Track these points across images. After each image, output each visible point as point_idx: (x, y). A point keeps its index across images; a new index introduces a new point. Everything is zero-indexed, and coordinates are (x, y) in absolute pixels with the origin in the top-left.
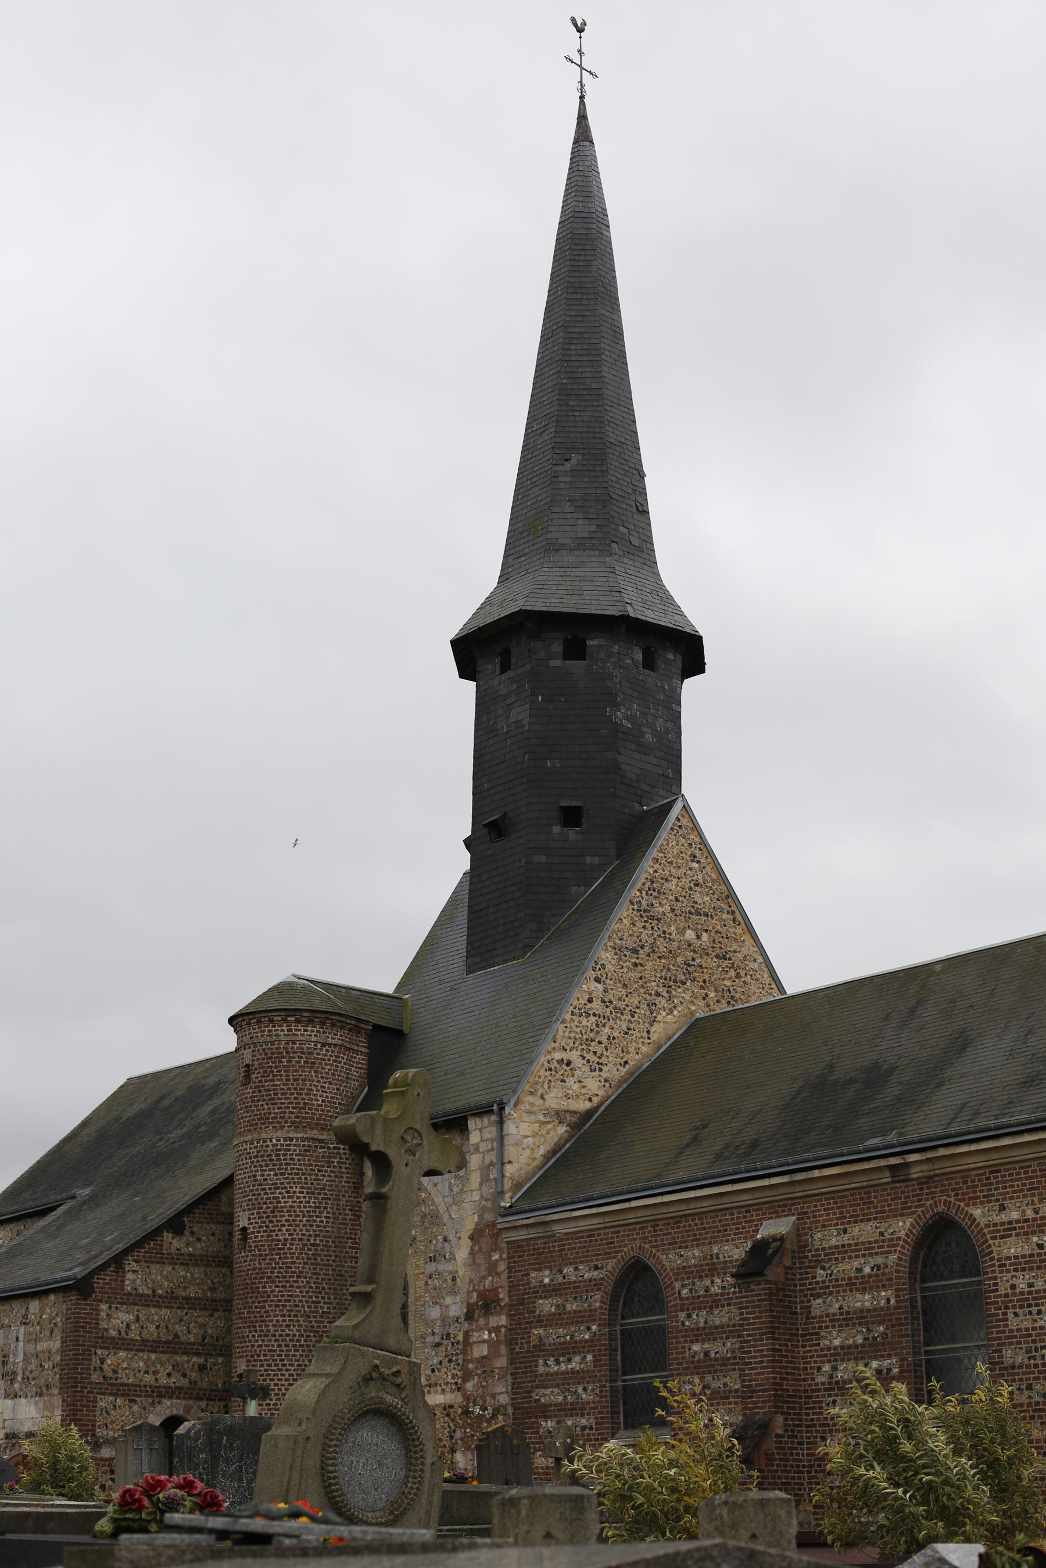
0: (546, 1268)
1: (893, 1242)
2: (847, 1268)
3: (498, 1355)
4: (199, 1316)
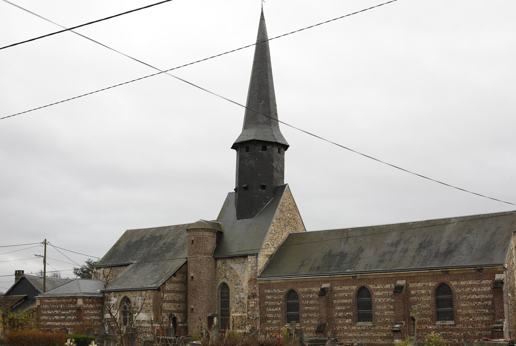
1: (352, 290)
2: (342, 294)
3: (257, 307)
4: (178, 295)
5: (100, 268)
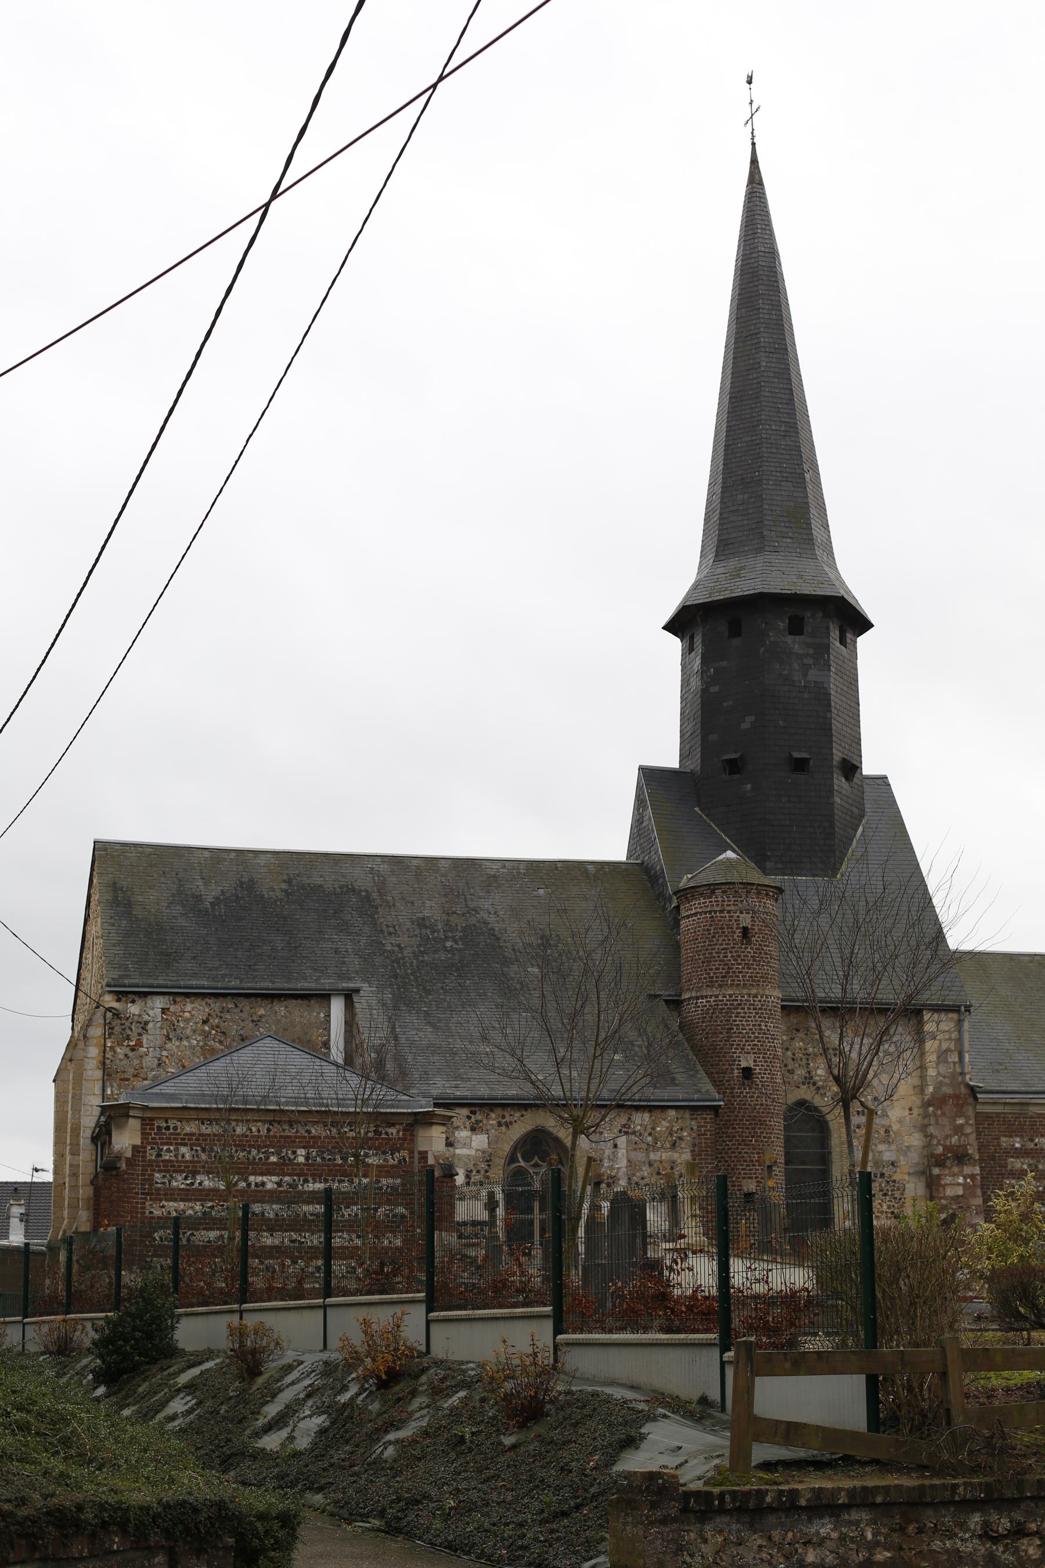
0: (1016, 1136)
5: (145, 995)
